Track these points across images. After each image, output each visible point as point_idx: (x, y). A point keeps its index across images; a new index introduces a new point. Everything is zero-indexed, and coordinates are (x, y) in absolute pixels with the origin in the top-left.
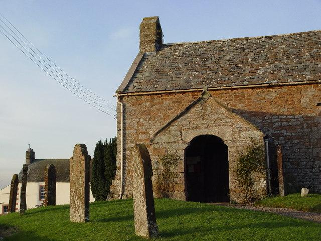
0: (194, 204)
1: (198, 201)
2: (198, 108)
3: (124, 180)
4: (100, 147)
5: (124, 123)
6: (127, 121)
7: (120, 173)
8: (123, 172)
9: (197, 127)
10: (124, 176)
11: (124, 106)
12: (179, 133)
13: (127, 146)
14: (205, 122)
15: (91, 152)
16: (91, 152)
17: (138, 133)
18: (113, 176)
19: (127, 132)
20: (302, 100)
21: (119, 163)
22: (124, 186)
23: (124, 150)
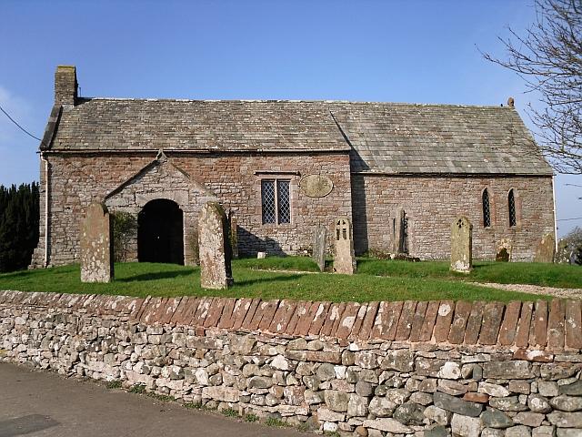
0: (148, 267)
1: (152, 261)
2: (154, 171)
3: (49, 249)
4: (21, 187)
5: (49, 184)
6: (53, 182)
7: (43, 241)
8: (48, 240)
9: (152, 191)
10: (49, 244)
11: (49, 165)
12: (133, 196)
13: (53, 210)
14: (160, 185)
15: (17, 189)
16: (17, 189)
17: (65, 195)
18: (35, 243)
19: (53, 194)
20: (242, 168)
21: (43, 229)
22: (48, 255)
23: (50, 215)
